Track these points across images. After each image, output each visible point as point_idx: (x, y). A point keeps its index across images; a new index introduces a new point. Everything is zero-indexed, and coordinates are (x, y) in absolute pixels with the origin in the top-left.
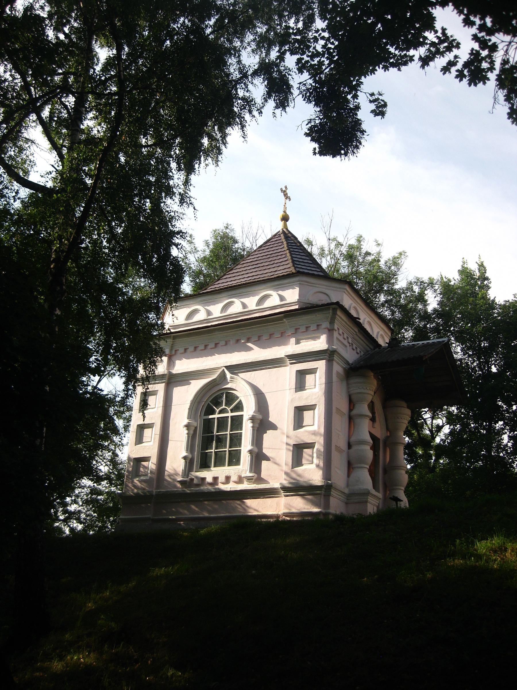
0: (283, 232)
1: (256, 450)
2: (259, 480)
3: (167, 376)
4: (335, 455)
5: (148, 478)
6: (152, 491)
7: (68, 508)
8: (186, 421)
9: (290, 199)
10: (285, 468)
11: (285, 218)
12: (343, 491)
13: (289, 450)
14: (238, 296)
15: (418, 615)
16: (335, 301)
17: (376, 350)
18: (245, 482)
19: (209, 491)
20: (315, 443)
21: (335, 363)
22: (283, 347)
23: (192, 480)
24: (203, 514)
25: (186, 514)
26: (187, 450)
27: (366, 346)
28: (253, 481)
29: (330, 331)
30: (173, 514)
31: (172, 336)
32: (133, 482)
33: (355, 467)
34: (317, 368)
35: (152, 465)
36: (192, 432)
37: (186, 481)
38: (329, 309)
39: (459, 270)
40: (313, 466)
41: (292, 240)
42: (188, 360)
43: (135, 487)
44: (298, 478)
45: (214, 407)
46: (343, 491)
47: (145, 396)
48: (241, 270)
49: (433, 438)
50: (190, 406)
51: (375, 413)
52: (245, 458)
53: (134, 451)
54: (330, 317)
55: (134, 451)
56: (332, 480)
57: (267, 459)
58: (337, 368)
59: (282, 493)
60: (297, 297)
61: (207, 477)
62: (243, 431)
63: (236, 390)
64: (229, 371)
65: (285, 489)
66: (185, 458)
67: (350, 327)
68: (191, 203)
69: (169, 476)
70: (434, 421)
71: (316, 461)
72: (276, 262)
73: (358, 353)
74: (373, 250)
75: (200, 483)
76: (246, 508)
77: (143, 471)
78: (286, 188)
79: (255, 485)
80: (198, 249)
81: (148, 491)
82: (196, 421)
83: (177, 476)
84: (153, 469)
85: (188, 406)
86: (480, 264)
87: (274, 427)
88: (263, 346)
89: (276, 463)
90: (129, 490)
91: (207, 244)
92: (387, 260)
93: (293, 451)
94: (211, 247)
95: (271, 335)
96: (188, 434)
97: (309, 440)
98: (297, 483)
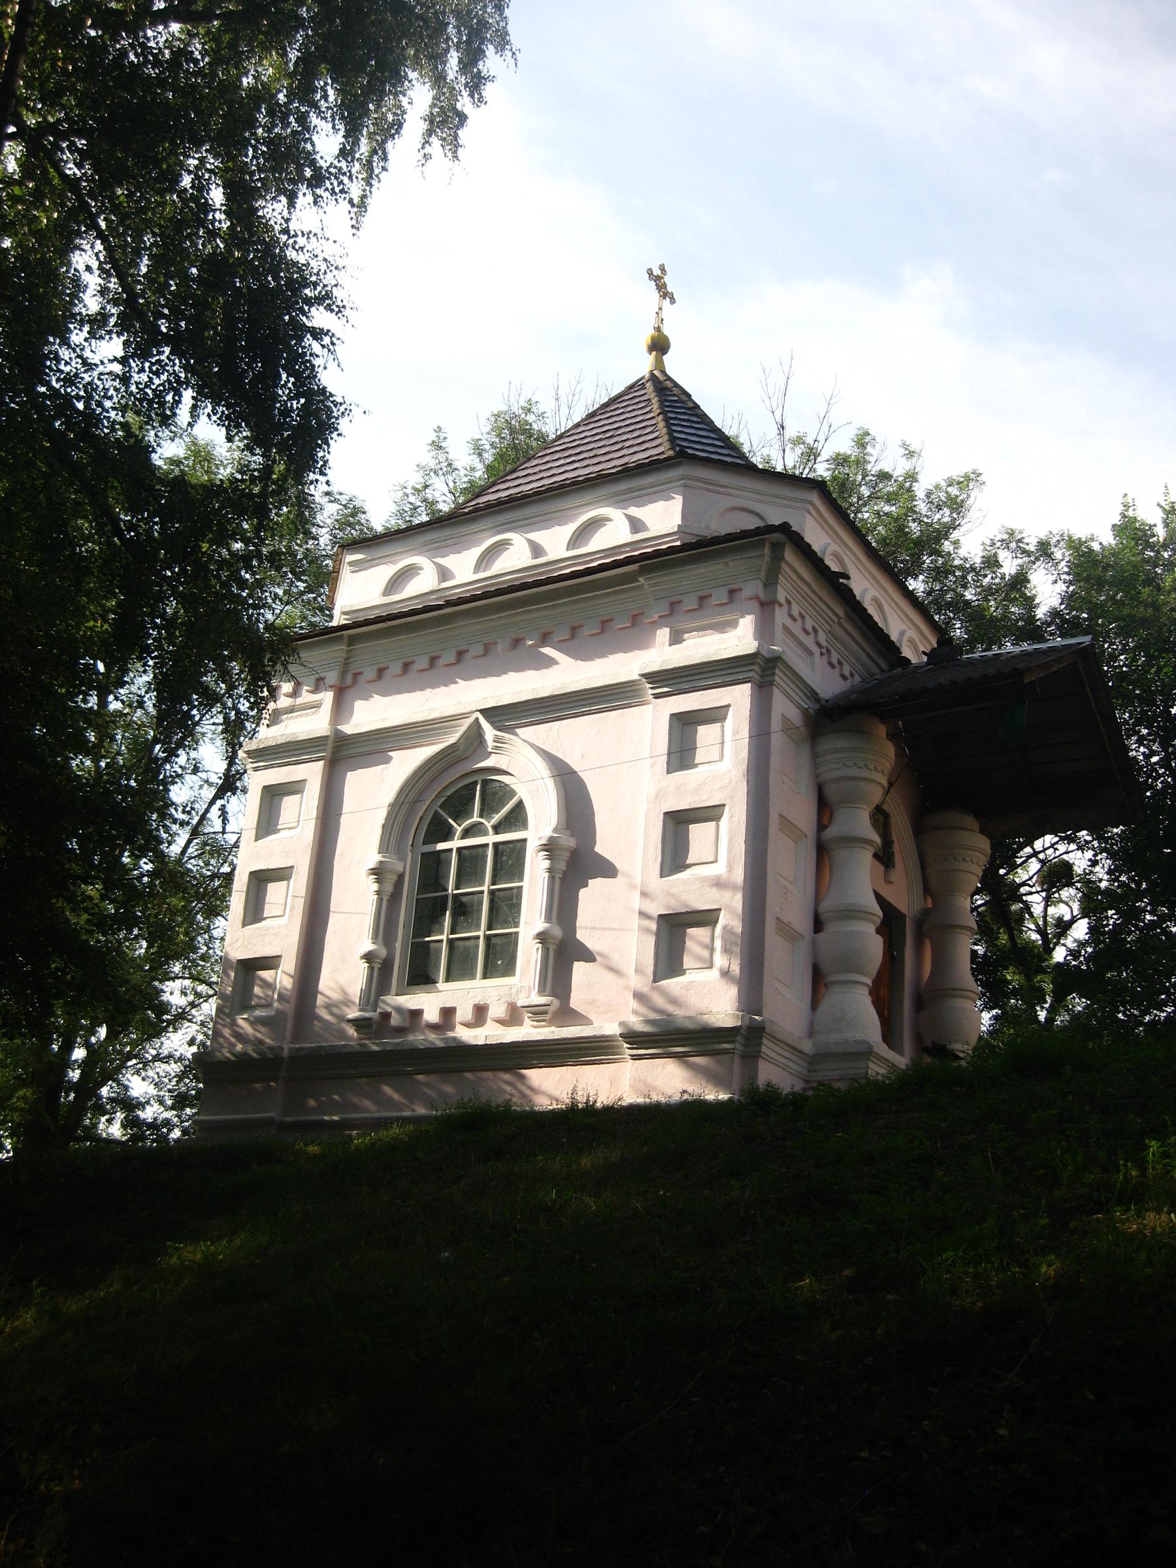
0: (653, 377)
1: (558, 932)
2: (566, 1014)
3: (330, 742)
4: (775, 945)
5: (273, 1013)
6: (281, 1048)
7: (139, 1113)
8: (374, 858)
9: (673, 301)
10: (642, 983)
11: (659, 346)
12: (798, 1047)
13: (648, 930)
14: (521, 526)
15: (1002, 1432)
16: (777, 522)
17: (894, 671)
18: (527, 1022)
19: (428, 1045)
20: (719, 910)
21: (777, 693)
22: (637, 653)
23: (386, 1016)
24: (413, 1110)
25: (370, 1109)
26: (375, 937)
27: (870, 663)
28: (547, 1017)
29: (766, 607)
30: (337, 1108)
31: (345, 639)
32: (234, 1023)
33: (832, 983)
34: (728, 706)
35: (283, 978)
36: (389, 888)
37: (370, 1019)
38: (761, 544)
39: (1114, 526)
40: (714, 974)
41: (675, 395)
42: (387, 698)
43: (239, 1037)
44: (670, 1008)
45: (450, 821)
46: (797, 1046)
47: (273, 795)
48: (536, 469)
49: (1048, 949)
50: (386, 819)
51: (892, 842)
52: (529, 955)
53: (239, 943)
54: (765, 566)
55: (239, 943)
56: (764, 1013)
57: (588, 956)
58: (785, 708)
59: (626, 1050)
60: (677, 520)
61: (425, 1007)
62: (525, 884)
63: (512, 775)
64: (492, 723)
65: (634, 1038)
66: (368, 957)
67: (821, 599)
68: (342, 191)
69: (328, 1007)
70: (1051, 910)
71: (720, 960)
72: (627, 444)
73: (844, 677)
74: (898, 467)
75: (407, 1025)
76: (528, 1092)
77: (261, 995)
78: (662, 269)
79: (553, 1028)
80: (456, 464)
81: (271, 1048)
82: (402, 858)
83: (348, 1006)
84: (286, 989)
85: (381, 816)
86: (1167, 508)
87: (607, 870)
88: (582, 654)
89: (611, 969)
90: (223, 1047)
91: (479, 451)
92: (932, 488)
93: (658, 934)
94: (489, 457)
95: (605, 624)
96: (378, 893)
97: (702, 902)
98: (666, 1022)
